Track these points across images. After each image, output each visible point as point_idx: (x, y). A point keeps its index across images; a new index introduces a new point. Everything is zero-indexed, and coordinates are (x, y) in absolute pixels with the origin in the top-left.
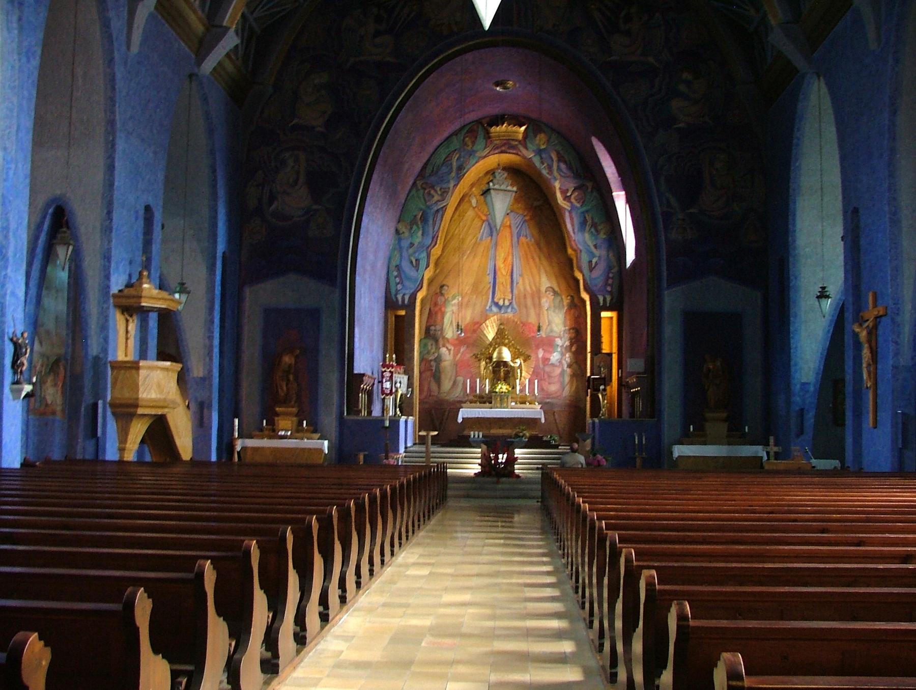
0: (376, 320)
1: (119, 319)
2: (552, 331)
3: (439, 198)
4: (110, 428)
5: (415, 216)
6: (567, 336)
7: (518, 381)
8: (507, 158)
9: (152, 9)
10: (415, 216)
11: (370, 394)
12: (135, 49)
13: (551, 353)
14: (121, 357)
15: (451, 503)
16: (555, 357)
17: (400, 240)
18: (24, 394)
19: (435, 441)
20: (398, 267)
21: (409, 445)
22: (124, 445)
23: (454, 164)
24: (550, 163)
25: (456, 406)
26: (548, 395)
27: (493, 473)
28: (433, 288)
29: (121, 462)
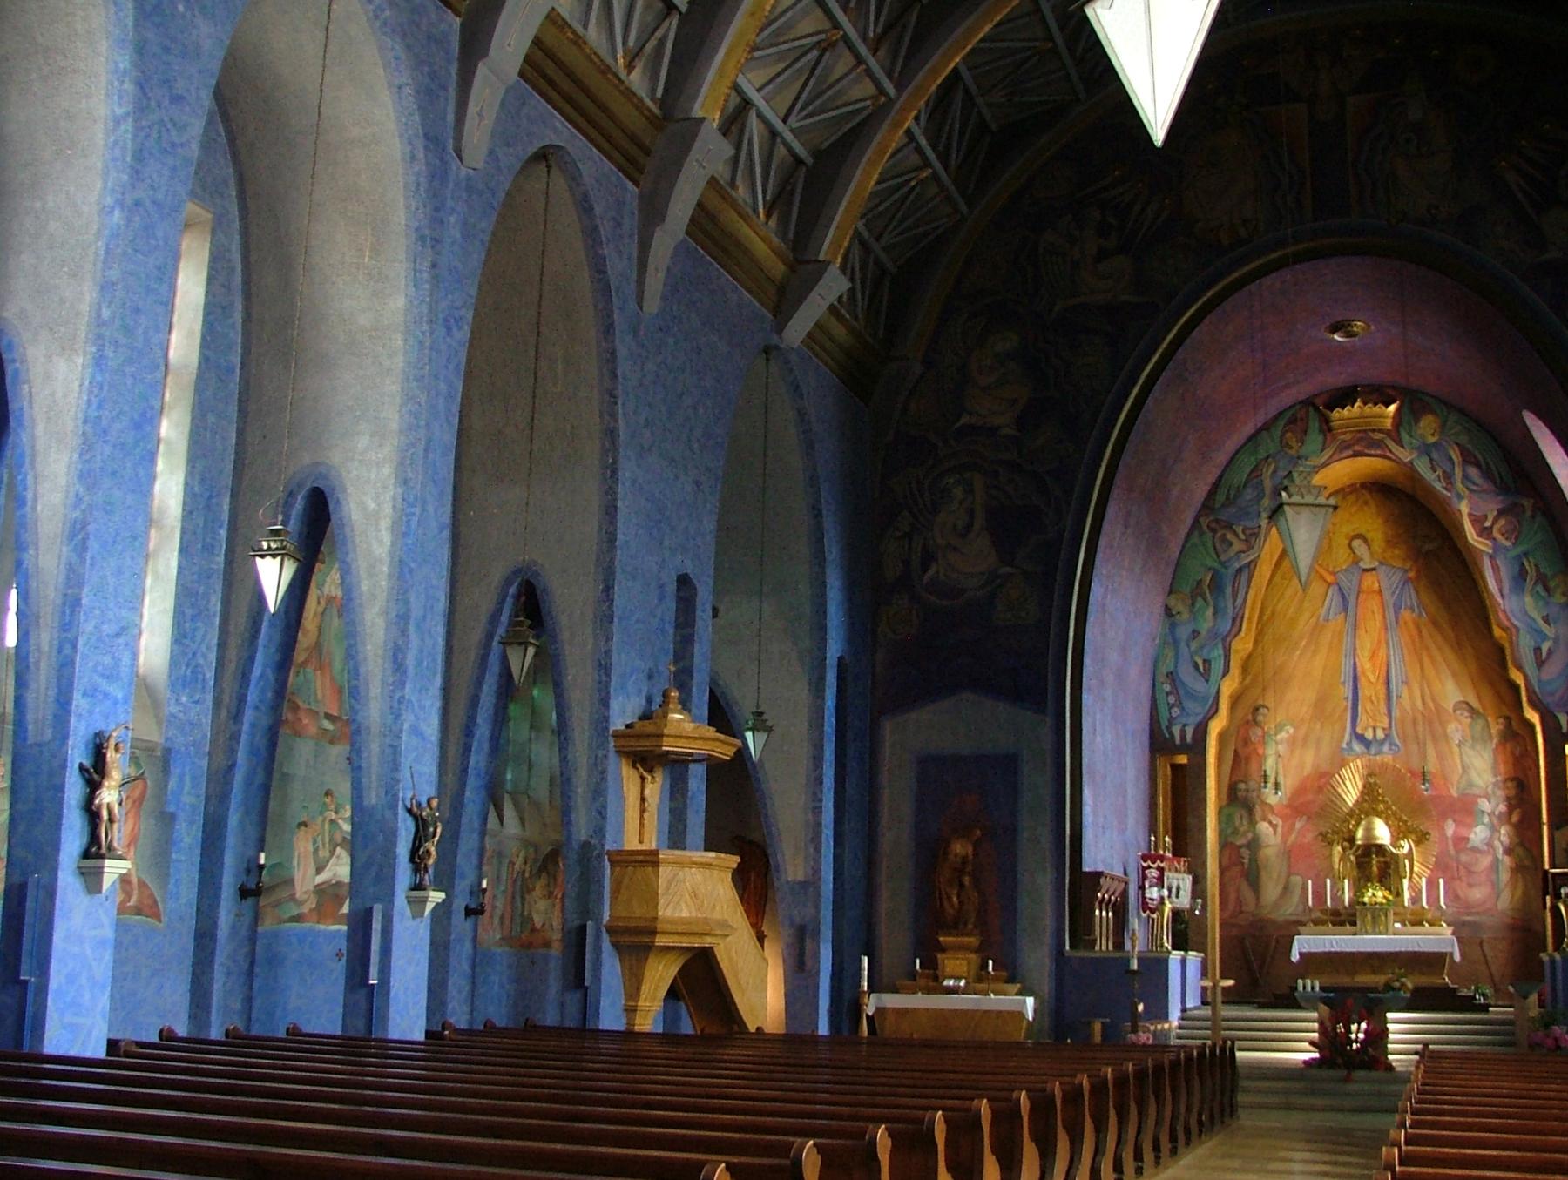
0: (1131, 774)
1: (628, 776)
2: (1470, 784)
3: (1244, 547)
4: (610, 969)
5: (1200, 582)
6: (1500, 793)
7: (1406, 882)
8: (1368, 465)
9: (682, 235)
10: (1200, 582)
11: (1120, 911)
12: (652, 305)
13: (1471, 827)
14: (631, 843)
15: (1246, 1119)
16: (1479, 834)
17: (1173, 626)
18: (429, 907)
19: (1232, 997)
20: (1172, 676)
21: (1189, 1005)
22: (636, 1002)
23: (1268, 485)
24: (1447, 468)
25: (1292, 928)
26: (1469, 907)
27: (1340, 1061)
28: (1241, 712)
29: (629, 1035)
